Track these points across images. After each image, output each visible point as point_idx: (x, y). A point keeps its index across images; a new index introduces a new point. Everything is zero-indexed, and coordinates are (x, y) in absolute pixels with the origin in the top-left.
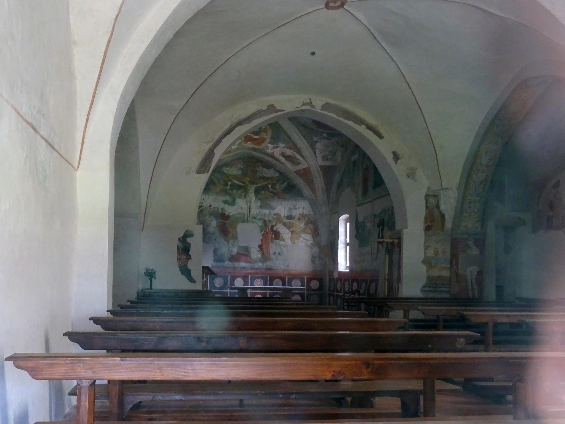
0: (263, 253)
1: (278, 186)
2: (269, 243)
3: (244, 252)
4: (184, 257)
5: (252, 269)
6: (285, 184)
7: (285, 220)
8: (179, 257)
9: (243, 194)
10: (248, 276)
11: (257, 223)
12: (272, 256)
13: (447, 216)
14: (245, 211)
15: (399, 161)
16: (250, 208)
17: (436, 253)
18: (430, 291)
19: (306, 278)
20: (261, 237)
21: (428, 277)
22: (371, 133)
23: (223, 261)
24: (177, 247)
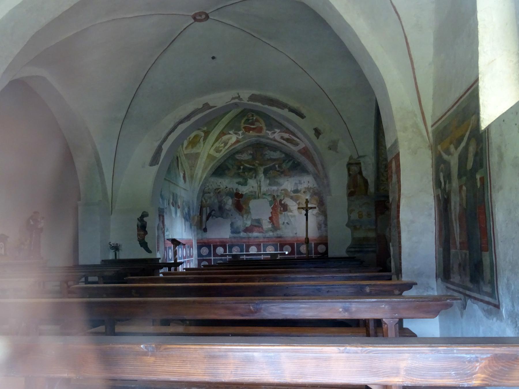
0: (273, 224)
1: (284, 166)
2: (278, 215)
3: (257, 224)
4: (142, 233)
5: (264, 238)
6: (290, 163)
7: (292, 194)
8: (139, 233)
9: (254, 175)
10: (261, 244)
11: (266, 198)
12: (281, 226)
13: (369, 181)
14: (256, 190)
15: (321, 136)
16: (260, 187)
17: (360, 216)
18: (355, 251)
19: (295, 243)
20: (271, 211)
21: (353, 239)
22: (294, 114)
23: (239, 233)
24: (137, 225)
